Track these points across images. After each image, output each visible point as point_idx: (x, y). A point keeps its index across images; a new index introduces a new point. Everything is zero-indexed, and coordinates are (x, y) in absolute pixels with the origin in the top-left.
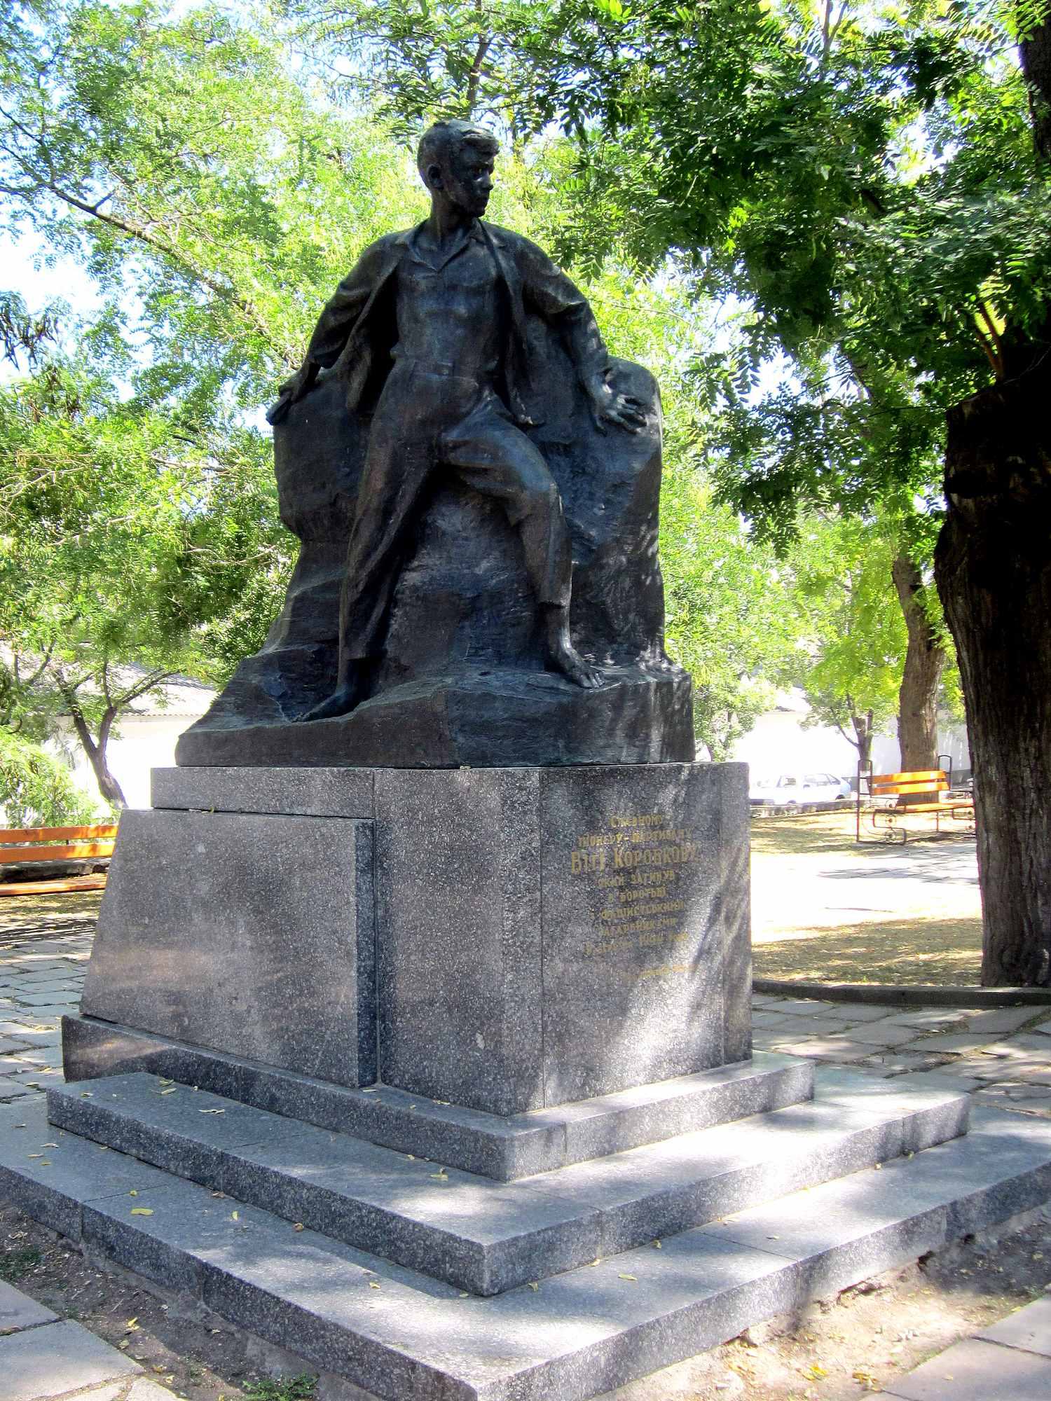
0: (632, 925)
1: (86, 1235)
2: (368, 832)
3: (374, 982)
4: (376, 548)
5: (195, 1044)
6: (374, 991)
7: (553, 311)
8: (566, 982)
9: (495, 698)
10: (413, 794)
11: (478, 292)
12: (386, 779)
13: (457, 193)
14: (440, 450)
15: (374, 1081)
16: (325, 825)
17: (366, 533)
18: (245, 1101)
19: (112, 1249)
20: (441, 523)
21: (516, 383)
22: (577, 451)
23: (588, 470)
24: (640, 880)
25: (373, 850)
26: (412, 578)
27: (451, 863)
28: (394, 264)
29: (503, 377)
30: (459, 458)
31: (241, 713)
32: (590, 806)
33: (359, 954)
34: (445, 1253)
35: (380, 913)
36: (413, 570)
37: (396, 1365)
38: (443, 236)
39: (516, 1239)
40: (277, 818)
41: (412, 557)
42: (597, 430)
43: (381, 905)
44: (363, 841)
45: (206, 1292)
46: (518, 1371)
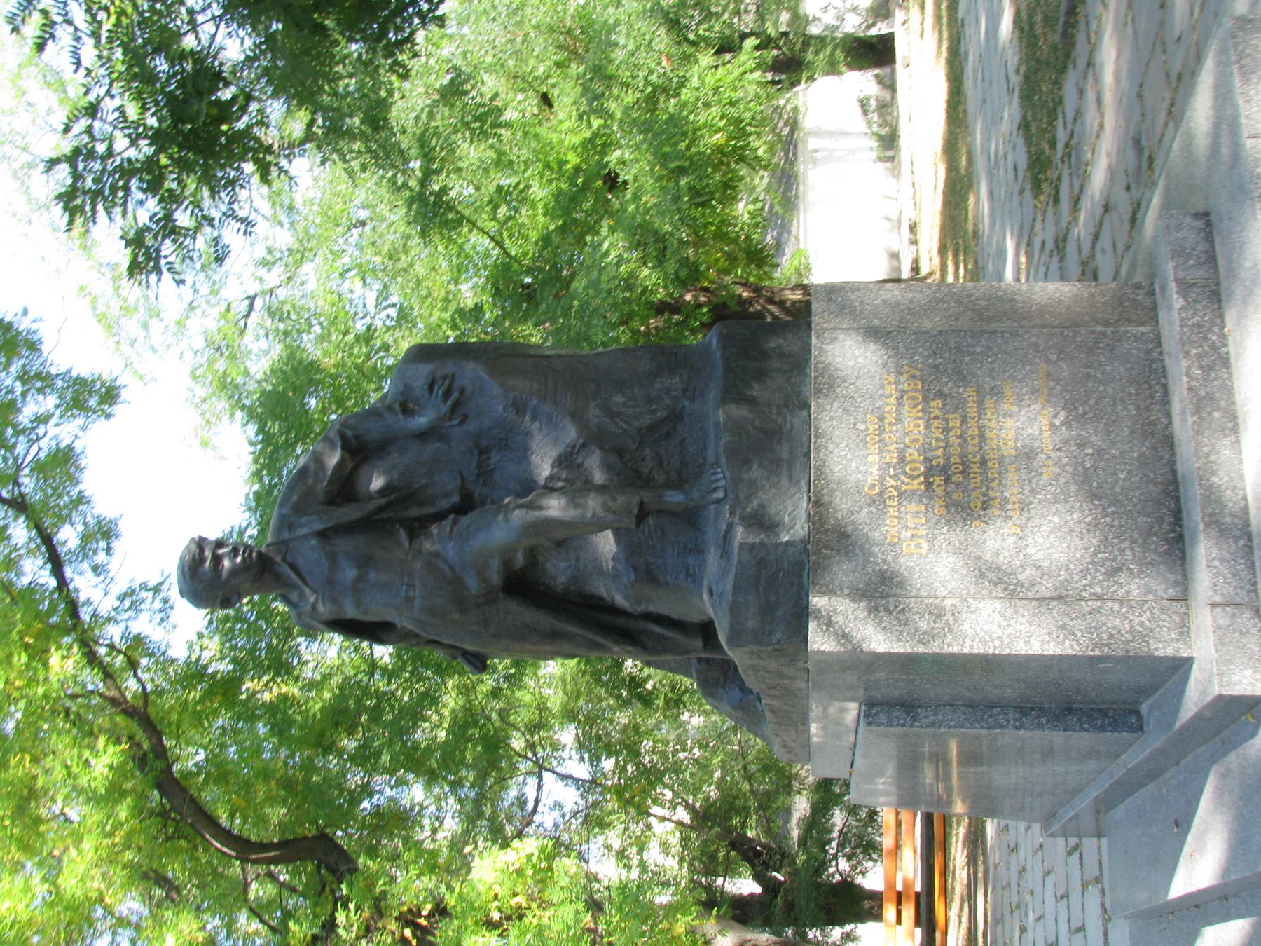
0: (990, 464)
2: (874, 711)
3: (1032, 709)
6: (1042, 709)
9: (734, 602)
11: (333, 559)
21: (421, 504)
30: (496, 578)
41: (601, 599)
44: (883, 718)
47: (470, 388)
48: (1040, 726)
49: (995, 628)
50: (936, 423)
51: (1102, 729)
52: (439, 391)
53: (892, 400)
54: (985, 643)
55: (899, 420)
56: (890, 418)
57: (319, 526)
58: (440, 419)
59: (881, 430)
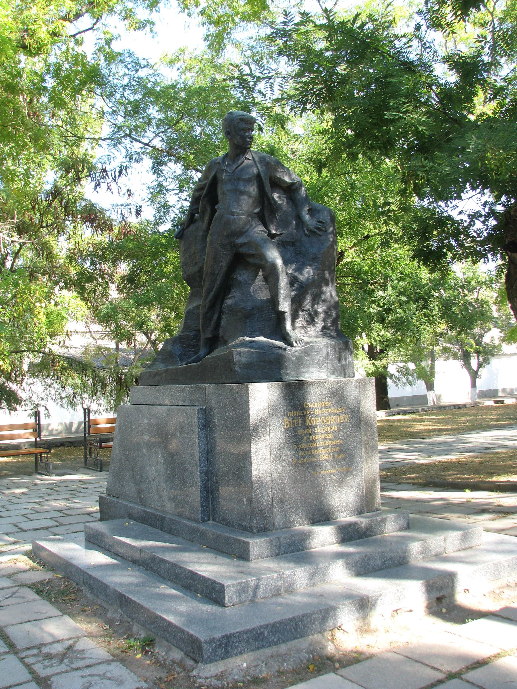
1: (85, 583)
4: (212, 290)
5: (145, 506)
6: (208, 481)
7: (285, 185)
8: (284, 475)
10: (219, 395)
12: (209, 388)
13: (238, 140)
14: (235, 247)
15: (209, 520)
16: (187, 409)
17: (207, 284)
18: (162, 530)
19: (92, 589)
20: (240, 278)
22: (298, 244)
23: (302, 252)
24: (319, 431)
25: (206, 419)
26: (229, 302)
27: (233, 424)
28: (215, 171)
29: (263, 215)
30: (243, 250)
31: (164, 363)
32: (294, 398)
33: (200, 465)
34: (213, 589)
35: (209, 447)
36: (229, 298)
37: (179, 632)
38: (234, 158)
39: (241, 583)
40: (173, 407)
41: (229, 293)
42: (306, 235)
43: (209, 443)
45: (121, 605)
46: (223, 634)
47: (322, 238)
48: (201, 481)
49: (260, 456)
50: (329, 429)
51: (202, 506)
52: (320, 225)
53: (336, 411)
54: (255, 453)
55: (330, 414)
56: (330, 410)
57: (262, 175)
58: (307, 225)
59: (326, 407)
